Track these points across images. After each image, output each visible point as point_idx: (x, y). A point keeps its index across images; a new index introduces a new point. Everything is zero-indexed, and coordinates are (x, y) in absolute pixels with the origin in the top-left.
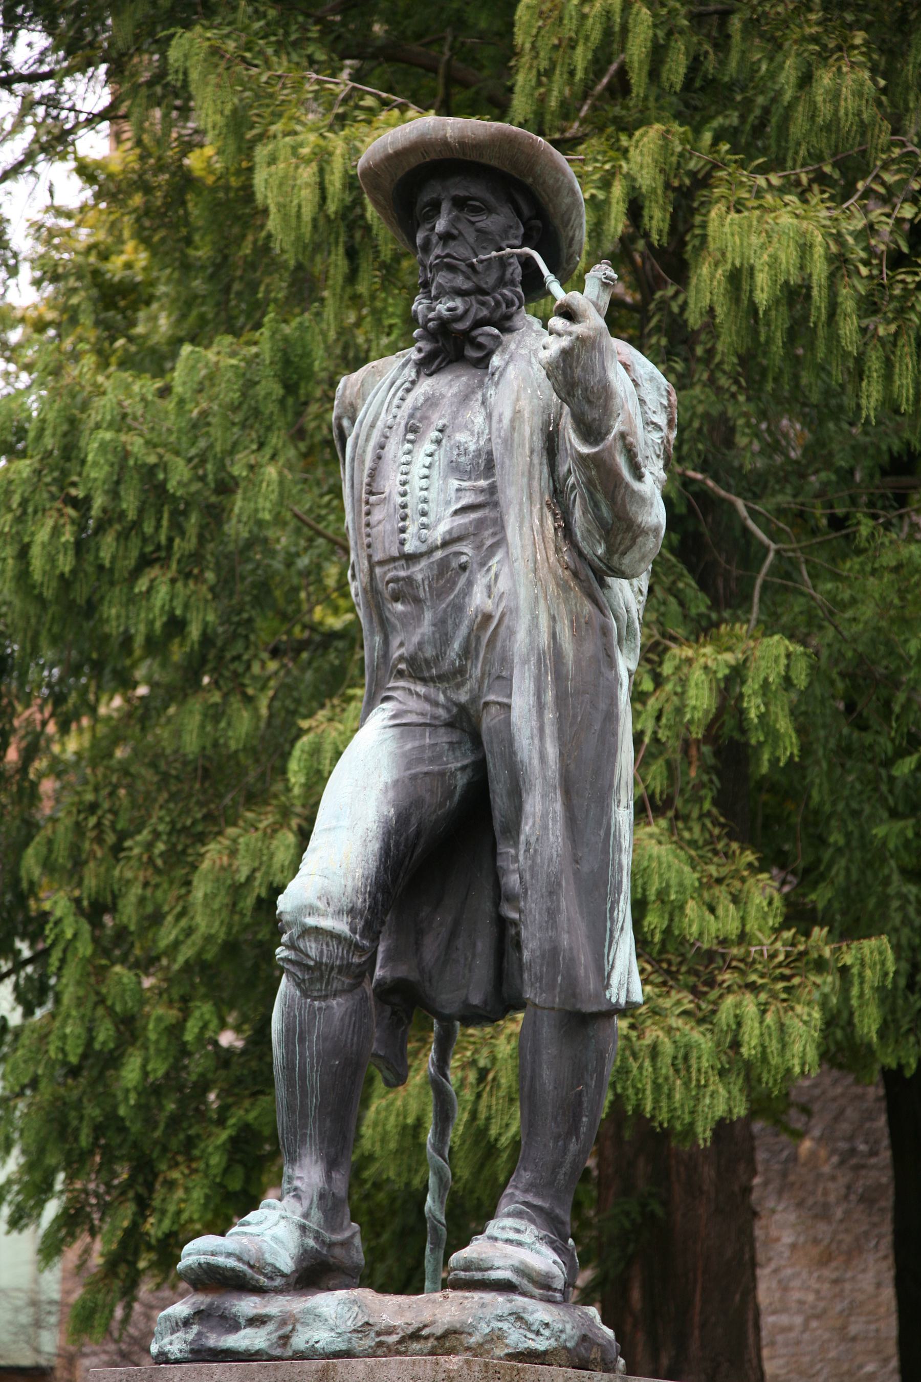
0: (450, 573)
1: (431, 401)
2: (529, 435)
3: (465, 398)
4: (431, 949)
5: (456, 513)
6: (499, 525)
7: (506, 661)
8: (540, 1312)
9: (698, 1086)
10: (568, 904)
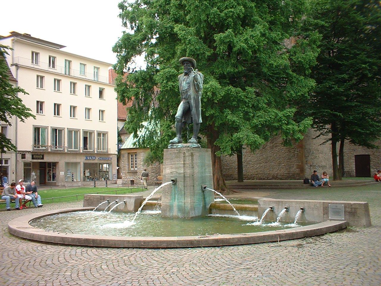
0: (187, 92)
1: (185, 78)
2: (192, 81)
3: (187, 78)
4: (187, 119)
6: (190, 88)
7: (191, 98)
8: (195, 145)
9: (244, 64)
10: (196, 116)
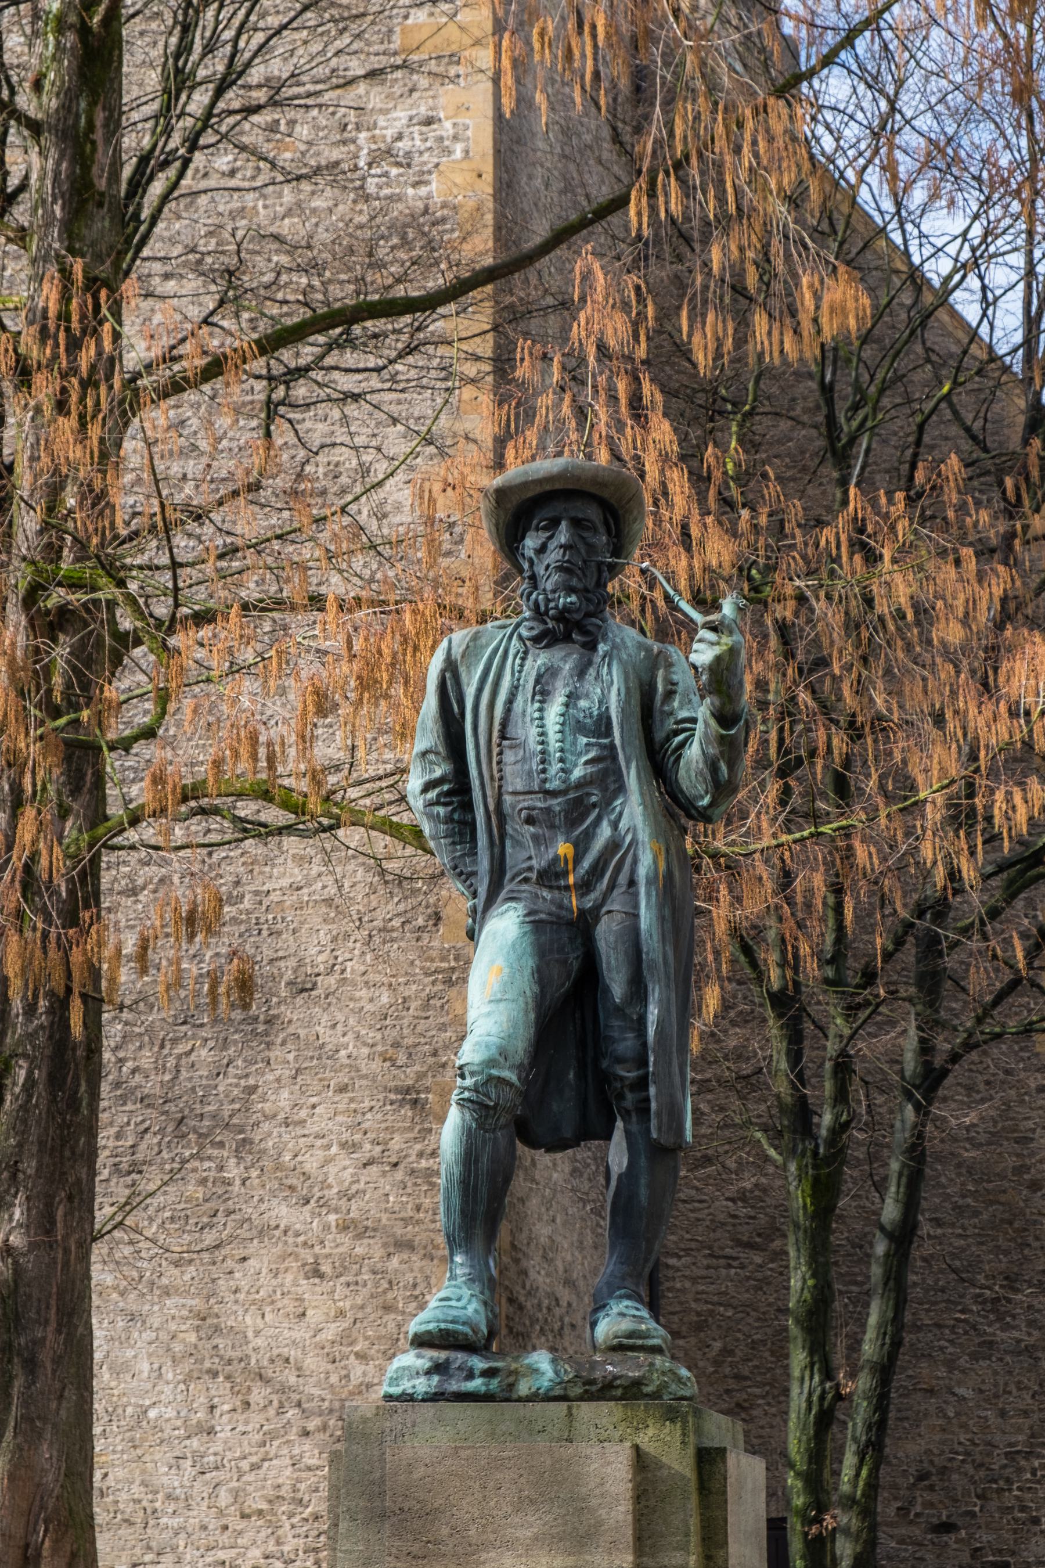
5: (586, 763)
